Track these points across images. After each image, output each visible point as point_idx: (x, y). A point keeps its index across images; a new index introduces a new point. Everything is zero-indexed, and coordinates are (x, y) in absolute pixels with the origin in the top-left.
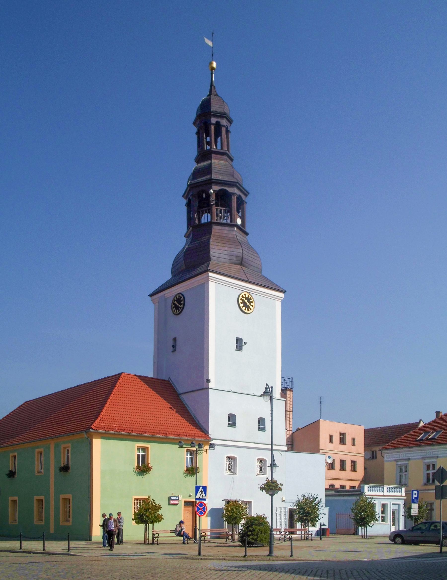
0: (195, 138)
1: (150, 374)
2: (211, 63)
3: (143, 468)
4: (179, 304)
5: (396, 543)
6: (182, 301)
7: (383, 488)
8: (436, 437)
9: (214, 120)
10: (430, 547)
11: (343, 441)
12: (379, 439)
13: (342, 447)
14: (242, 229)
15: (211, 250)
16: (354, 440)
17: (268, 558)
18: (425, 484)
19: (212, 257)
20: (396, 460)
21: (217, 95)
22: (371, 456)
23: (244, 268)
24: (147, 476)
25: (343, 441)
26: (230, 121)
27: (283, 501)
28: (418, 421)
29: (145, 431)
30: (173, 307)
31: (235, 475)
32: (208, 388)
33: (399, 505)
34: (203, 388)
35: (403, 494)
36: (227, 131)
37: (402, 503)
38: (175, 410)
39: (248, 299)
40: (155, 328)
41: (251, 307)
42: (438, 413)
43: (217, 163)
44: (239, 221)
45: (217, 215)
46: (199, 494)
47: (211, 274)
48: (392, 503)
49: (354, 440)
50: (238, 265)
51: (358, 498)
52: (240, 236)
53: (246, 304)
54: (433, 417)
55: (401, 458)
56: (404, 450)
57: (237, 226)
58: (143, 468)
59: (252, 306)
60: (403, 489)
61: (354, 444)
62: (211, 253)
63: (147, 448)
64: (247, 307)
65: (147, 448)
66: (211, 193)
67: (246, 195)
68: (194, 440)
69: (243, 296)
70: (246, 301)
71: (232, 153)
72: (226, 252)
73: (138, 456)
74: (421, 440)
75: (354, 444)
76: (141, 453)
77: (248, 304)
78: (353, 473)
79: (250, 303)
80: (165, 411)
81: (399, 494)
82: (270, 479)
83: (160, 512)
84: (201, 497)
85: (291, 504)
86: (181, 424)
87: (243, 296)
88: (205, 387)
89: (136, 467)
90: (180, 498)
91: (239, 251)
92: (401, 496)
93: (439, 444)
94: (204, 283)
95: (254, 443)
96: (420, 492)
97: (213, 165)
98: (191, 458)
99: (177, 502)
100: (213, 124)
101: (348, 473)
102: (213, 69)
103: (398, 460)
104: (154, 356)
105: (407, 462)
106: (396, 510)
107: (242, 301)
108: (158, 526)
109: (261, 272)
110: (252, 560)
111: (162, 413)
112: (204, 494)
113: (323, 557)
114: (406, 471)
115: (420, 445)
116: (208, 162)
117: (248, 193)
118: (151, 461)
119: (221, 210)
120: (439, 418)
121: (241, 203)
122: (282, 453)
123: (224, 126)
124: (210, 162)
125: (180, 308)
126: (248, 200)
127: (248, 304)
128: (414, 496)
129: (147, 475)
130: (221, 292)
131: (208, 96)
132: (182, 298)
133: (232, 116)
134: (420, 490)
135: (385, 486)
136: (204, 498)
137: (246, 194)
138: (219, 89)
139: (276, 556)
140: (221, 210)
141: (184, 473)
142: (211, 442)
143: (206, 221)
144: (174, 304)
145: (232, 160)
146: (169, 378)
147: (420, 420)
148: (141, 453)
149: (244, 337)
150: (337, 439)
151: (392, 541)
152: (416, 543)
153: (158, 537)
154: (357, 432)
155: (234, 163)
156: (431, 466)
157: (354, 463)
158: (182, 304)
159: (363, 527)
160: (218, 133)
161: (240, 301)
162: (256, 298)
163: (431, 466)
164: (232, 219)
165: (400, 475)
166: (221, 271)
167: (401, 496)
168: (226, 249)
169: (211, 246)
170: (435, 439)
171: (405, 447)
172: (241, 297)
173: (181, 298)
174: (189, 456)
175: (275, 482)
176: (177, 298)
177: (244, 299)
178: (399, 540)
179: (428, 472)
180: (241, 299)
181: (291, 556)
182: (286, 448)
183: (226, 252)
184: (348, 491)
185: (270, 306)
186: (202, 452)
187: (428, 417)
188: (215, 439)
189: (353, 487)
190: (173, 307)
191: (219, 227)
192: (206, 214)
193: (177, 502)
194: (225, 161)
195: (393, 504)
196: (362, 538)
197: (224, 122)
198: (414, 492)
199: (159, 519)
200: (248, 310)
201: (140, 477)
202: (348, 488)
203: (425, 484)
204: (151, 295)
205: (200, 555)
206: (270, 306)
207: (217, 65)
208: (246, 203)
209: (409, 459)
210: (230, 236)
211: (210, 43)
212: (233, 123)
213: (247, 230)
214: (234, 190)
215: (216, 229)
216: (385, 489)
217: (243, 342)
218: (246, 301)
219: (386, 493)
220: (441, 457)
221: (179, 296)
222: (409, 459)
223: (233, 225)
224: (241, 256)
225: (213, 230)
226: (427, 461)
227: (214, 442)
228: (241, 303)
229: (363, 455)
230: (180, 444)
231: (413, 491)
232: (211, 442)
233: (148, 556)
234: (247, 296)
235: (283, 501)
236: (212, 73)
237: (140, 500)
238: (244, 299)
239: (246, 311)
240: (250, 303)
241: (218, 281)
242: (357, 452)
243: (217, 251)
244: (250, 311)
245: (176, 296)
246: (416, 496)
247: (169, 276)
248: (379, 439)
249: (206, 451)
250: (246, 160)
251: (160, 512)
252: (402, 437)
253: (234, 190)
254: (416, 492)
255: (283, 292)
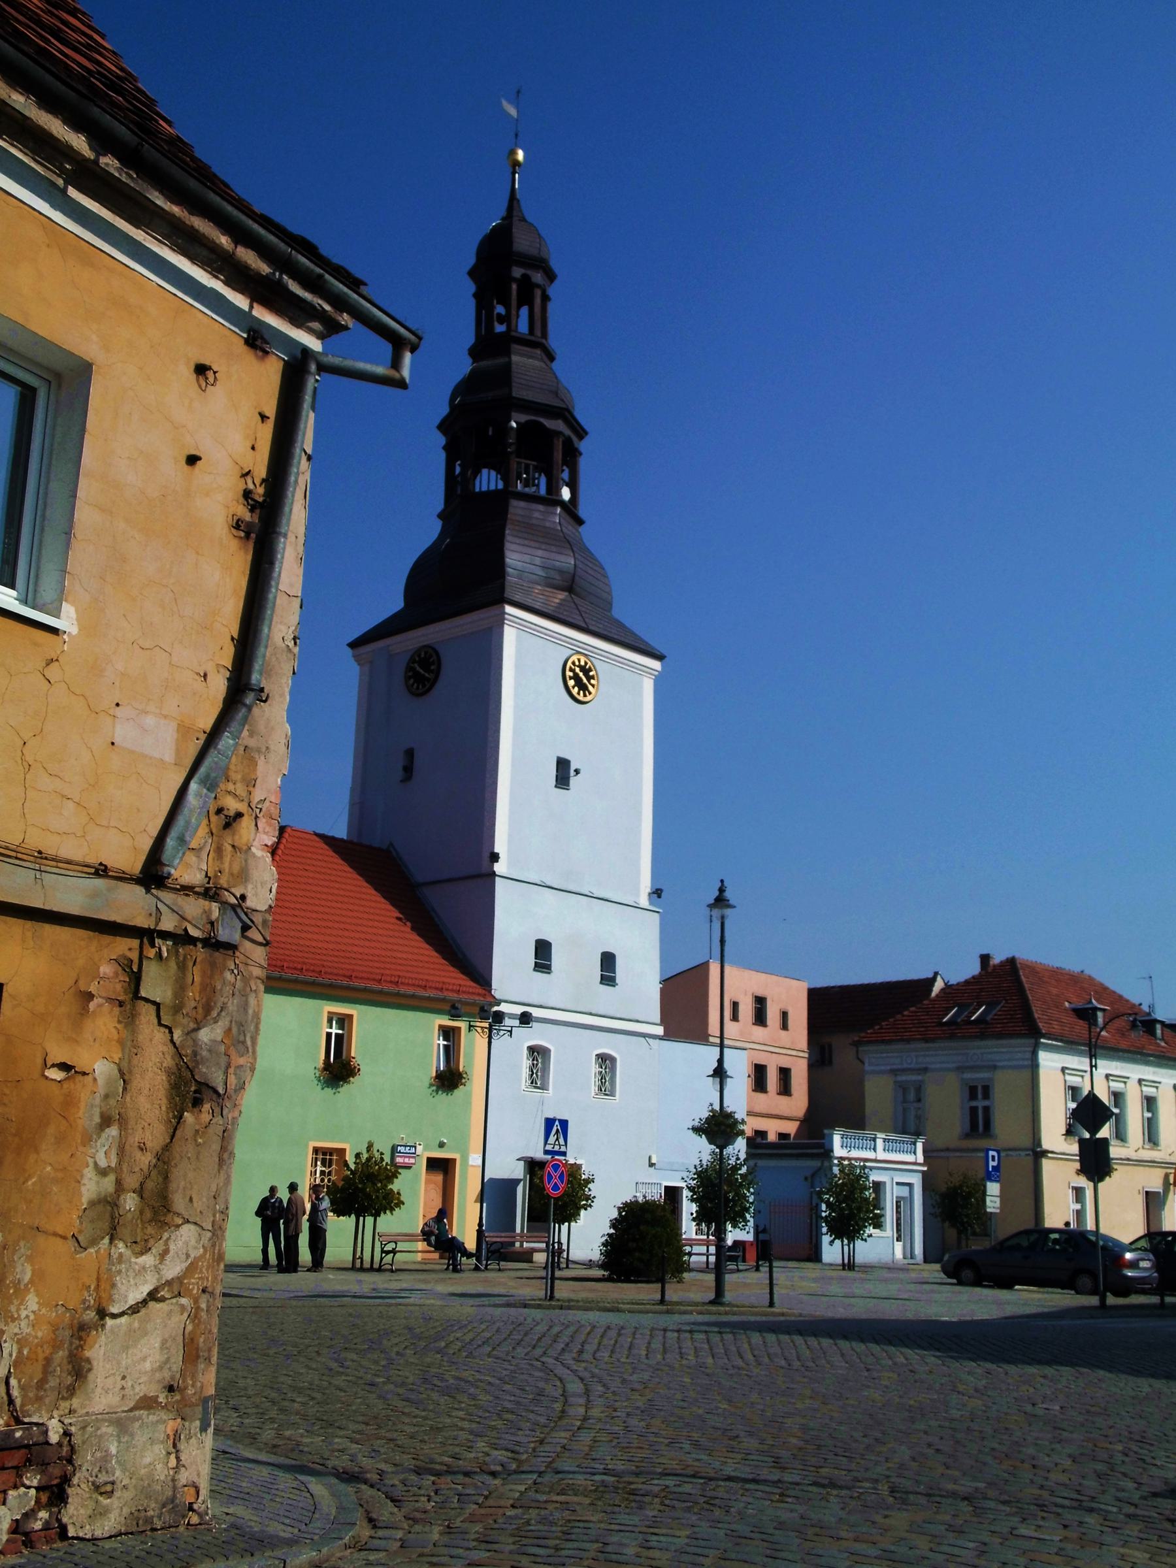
0: (470, 305)
1: (341, 831)
2: (513, 153)
3: (338, 1070)
4: (423, 672)
5: (960, 1283)
6: (433, 663)
7: (874, 1140)
8: (989, 1018)
9: (517, 272)
10: (1059, 1296)
11: (760, 1018)
12: (841, 1016)
13: (759, 1032)
14: (570, 509)
15: (508, 554)
16: (785, 1015)
17: (713, 1308)
18: (967, 1136)
19: (509, 570)
20: (894, 1072)
21: (523, 220)
22: (820, 1056)
23: (579, 602)
24: (345, 1089)
25: (760, 1018)
26: (551, 276)
27: (651, 1165)
28: (930, 975)
29: (349, 973)
30: (410, 677)
31: (545, 1094)
32: (493, 874)
33: (910, 1185)
34: (480, 874)
35: (920, 1158)
36: (545, 298)
37: (916, 1180)
38: (409, 924)
39: (586, 671)
40: (357, 725)
41: (590, 688)
42: (985, 959)
43: (522, 361)
44: (566, 493)
45: (519, 477)
46: (552, 1139)
47: (509, 609)
48: (896, 1180)
49: (785, 1015)
50: (563, 590)
51: (819, 1164)
52: (569, 528)
53: (581, 680)
54: (973, 969)
55: (905, 1066)
56: (913, 1046)
57: (562, 503)
58: (338, 1070)
59: (593, 686)
60: (920, 1146)
61: (785, 1026)
62: (508, 560)
63: (351, 1017)
64: (583, 687)
65: (351, 1017)
66: (512, 428)
67: (581, 438)
68: (460, 1001)
69: (573, 663)
70: (581, 674)
71: (554, 342)
72: (538, 561)
73: (329, 1035)
74: (951, 1022)
75: (785, 1026)
76: (335, 1031)
77: (585, 680)
78: (784, 1099)
79: (589, 678)
80: (386, 926)
81: (910, 1158)
82: (717, 1107)
83: (395, 1186)
84: (557, 1148)
85: (685, 1174)
86: (426, 959)
87: (573, 663)
88: (484, 870)
89: (321, 1064)
90: (420, 1149)
91: (567, 561)
92: (915, 1164)
93: (1000, 1036)
94: (490, 628)
95: (591, 1014)
96: (1003, 1154)
97: (514, 366)
98: (446, 1048)
99: (412, 1161)
100: (515, 280)
101: (771, 1100)
102: (516, 163)
103: (899, 1070)
104: (353, 790)
105: (920, 1078)
106: (903, 1198)
107: (571, 674)
108: (388, 1223)
109: (610, 610)
110: (685, 1313)
111: (381, 931)
112: (562, 1141)
113: (841, 1310)
114: (919, 1100)
115: (952, 1037)
116: (502, 360)
117: (586, 433)
118: (356, 1050)
119: (527, 466)
120: (990, 970)
121: (571, 455)
122: (651, 1041)
123: (538, 286)
124: (507, 359)
125: (428, 680)
126: (583, 446)
127: (585, 680)
128: (992, 1164)
129: (346, 1086)
130: (528, 651)
131: (503, 219)
132: (435, 657)
133: (555, 264)
134: (1005, 1150)
135: (879, 1135)
136: (563, 1149)
137: (581, 433)
138: (529, 209)
139: (729, 1305)
140: (527, 466)
141: (431, 1085)
142: (496, 1008)
143: (484, 488)
144: (413, 669)
145: (552, 358)
146: (391, 844)
147: (936, 974)
148: (335, 1031)
149: (574, 755)
150: (747, 1010)
151: (949, 1277)
152: (1006, 1283)
153: (394, 1252)
154: (790, 996)
155: (555, 365)
156: (980, 1088)
157: (785, 1073)
158: (432, 671)
159: (846, 1241)
160: (526, 298)
161: (569, 674)
162: (601, 668)
163: (980, 1088)
164: (553, 489)
165: (904, 1110)
166: (529, 602)
167: (915, 1164)
168: (540, 553)
169: (507, 545)
170: (986, 1022)
171: (914, 1040)
172: (569, 664)
173: (431, 656)
174: (442, 1042)
175: (730, 1115)
176: (419, 656)
177: (577, 670)
178: (967, 1274)
179: (974, 1104)
180: (571, 670)
181: (771, 1304)
182: (660, 1030)
183: (538, 561)
184: (772, 1145)
185: (630, 685)
186: (502, 1033)
187: (959, 968)
188: (506, 1001)
189: (783, 1136)
190: (410, 677)
191: (522, 504)
192: (485, 471)
193: (412, 1161)
194: (537, 359)
195: (898, 1184)
196: (844, 1269)
197: (538, 277)
198: (991, 1153)
199: (391, 1202)
200: (585, 695)
201: (329, 1091)
202: (772, 1137)
203: (967, 1136)
204: (353, 645)
205: (552, 1298)
206: (630, 685)
207: (525, 157)
208: (581, 454)
209: (926, 1070)
210: (547, 524)
211: (513, 112)
212: (557, 282)
213: (582, 512)
214: (558, 425)
215: (517, 508)
216: (879, 1143)
217: (573, 768)
218: (581, 674)
219: (881, 1155)
220: (1003, 1067)
221: (426, 653)
222: (926, 1070)
223: (552, 499)
224: (572, 571)
225: (511, 510)
226: (968, 1075)
227: (503, 1008)
228: (571, 678)
229: (806, 1055)
230: (453, 1012)
231: (987, 1150)
232: (496, 1008)
233: (414, 1299)
234: (582, 663)
235: (651, 1165)
236: (514, 173)
237: (324, 1154)
238: (577, 670)
239: (581, 698)
240: (589, 678)
241: (521, 625)
242: (790, 1046)
243: (519, 559)
244: (589, 698)
245: (418, 652)
246: (995, 1164)
247: (397, 603)
248: (841, 1016)
249: (511, 1032)
250: (584, 359)
251: (395, 1186)
252: (906, 1013)
253: (558, 425)
254: (995, 1153)
255: (659, 657)
